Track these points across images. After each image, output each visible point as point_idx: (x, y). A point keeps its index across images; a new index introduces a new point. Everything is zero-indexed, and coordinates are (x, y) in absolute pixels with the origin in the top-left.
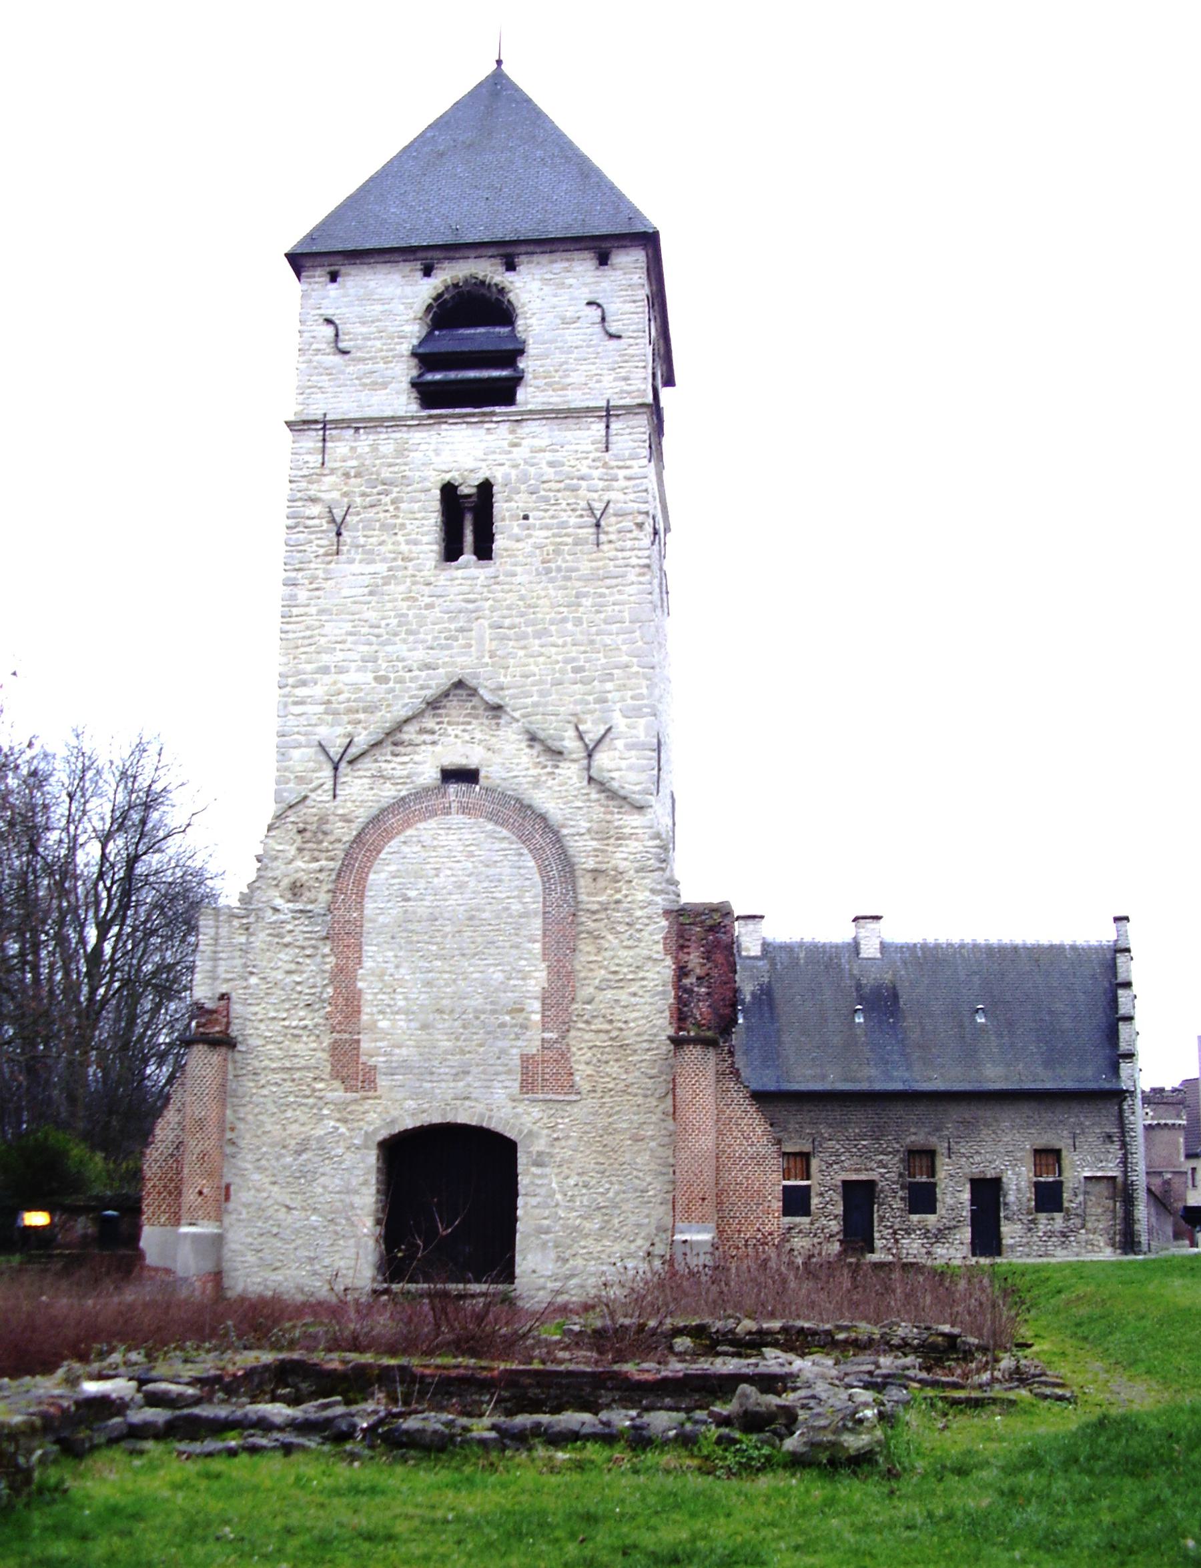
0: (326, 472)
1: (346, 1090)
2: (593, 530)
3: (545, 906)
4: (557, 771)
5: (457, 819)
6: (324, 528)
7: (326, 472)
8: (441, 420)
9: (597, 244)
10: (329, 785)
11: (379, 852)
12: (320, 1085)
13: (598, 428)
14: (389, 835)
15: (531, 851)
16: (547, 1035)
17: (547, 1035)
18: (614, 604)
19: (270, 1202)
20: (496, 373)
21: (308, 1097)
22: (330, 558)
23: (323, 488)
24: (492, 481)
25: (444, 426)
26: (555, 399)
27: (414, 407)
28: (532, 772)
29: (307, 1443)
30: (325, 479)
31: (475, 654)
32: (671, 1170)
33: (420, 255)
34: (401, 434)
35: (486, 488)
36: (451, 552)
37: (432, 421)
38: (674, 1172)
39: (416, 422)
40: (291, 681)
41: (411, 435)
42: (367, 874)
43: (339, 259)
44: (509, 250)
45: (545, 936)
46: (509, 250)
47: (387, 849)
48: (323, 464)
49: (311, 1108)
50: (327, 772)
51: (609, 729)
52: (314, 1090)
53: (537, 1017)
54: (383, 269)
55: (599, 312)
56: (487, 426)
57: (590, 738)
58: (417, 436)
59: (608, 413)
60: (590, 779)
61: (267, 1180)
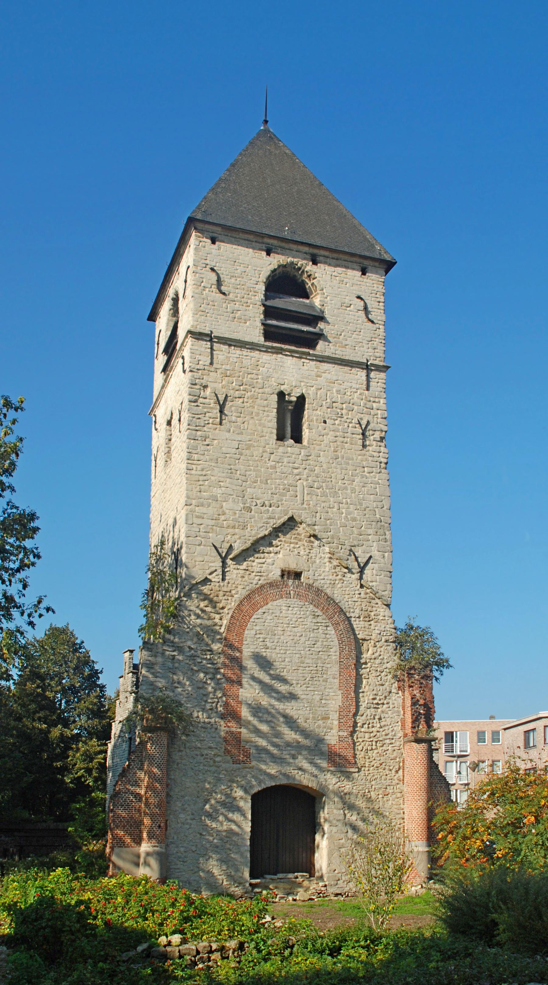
0: (213, 369)
1: (234, 763)
2: (361, 436)
3: (340, 658)
4: (344, 578)
5: (294, 601)
6: (211, 406)
7: (213, 369)
8: (279, 351)
9: (361, 260)
10: (220, 571)
11: (250, 617)
12: (218, 759)
13: (363, 373)
14: (255, 608)
15: (333, 625)
16: (341, 733)
17: (341, 733)
18: (371, 483)
19: (191, 831)
20: (305, 328)
21: (211, 766)
22: (215, 426)
23: (210, 380)
24: (306, 395)
25: (280, 356)
26: (340, 353)
27: (261, 340)
28: (331, 577)
29: (314, 959)
30: (211, 374)
31: (299, 502)
32: (402, 812)
33: (266, 240)
34: (256, 354)
35: (302, 399)
36: (281, 437)
37: (273, 351)
38: (404, 813)
39: (264, 349)
40: (194, 502)
41: (260, 356)
42: (244, 630)
43: (219, 229)
44: (316, 251)
45: (340, 676)
46: (316, 251)
47: (254, 616)
48: (211, 363)
49: (214, 773)
50: (218, 564)
51: (371, 557)
52: (215, 762)
53: (336, 723)
54: (182, 255)
55: (362, 303)
56: (303, 360)
57: (362, 560)
58: (266, 357)
59: (367, 367)
60: (362, 586)
61: (188, 817)
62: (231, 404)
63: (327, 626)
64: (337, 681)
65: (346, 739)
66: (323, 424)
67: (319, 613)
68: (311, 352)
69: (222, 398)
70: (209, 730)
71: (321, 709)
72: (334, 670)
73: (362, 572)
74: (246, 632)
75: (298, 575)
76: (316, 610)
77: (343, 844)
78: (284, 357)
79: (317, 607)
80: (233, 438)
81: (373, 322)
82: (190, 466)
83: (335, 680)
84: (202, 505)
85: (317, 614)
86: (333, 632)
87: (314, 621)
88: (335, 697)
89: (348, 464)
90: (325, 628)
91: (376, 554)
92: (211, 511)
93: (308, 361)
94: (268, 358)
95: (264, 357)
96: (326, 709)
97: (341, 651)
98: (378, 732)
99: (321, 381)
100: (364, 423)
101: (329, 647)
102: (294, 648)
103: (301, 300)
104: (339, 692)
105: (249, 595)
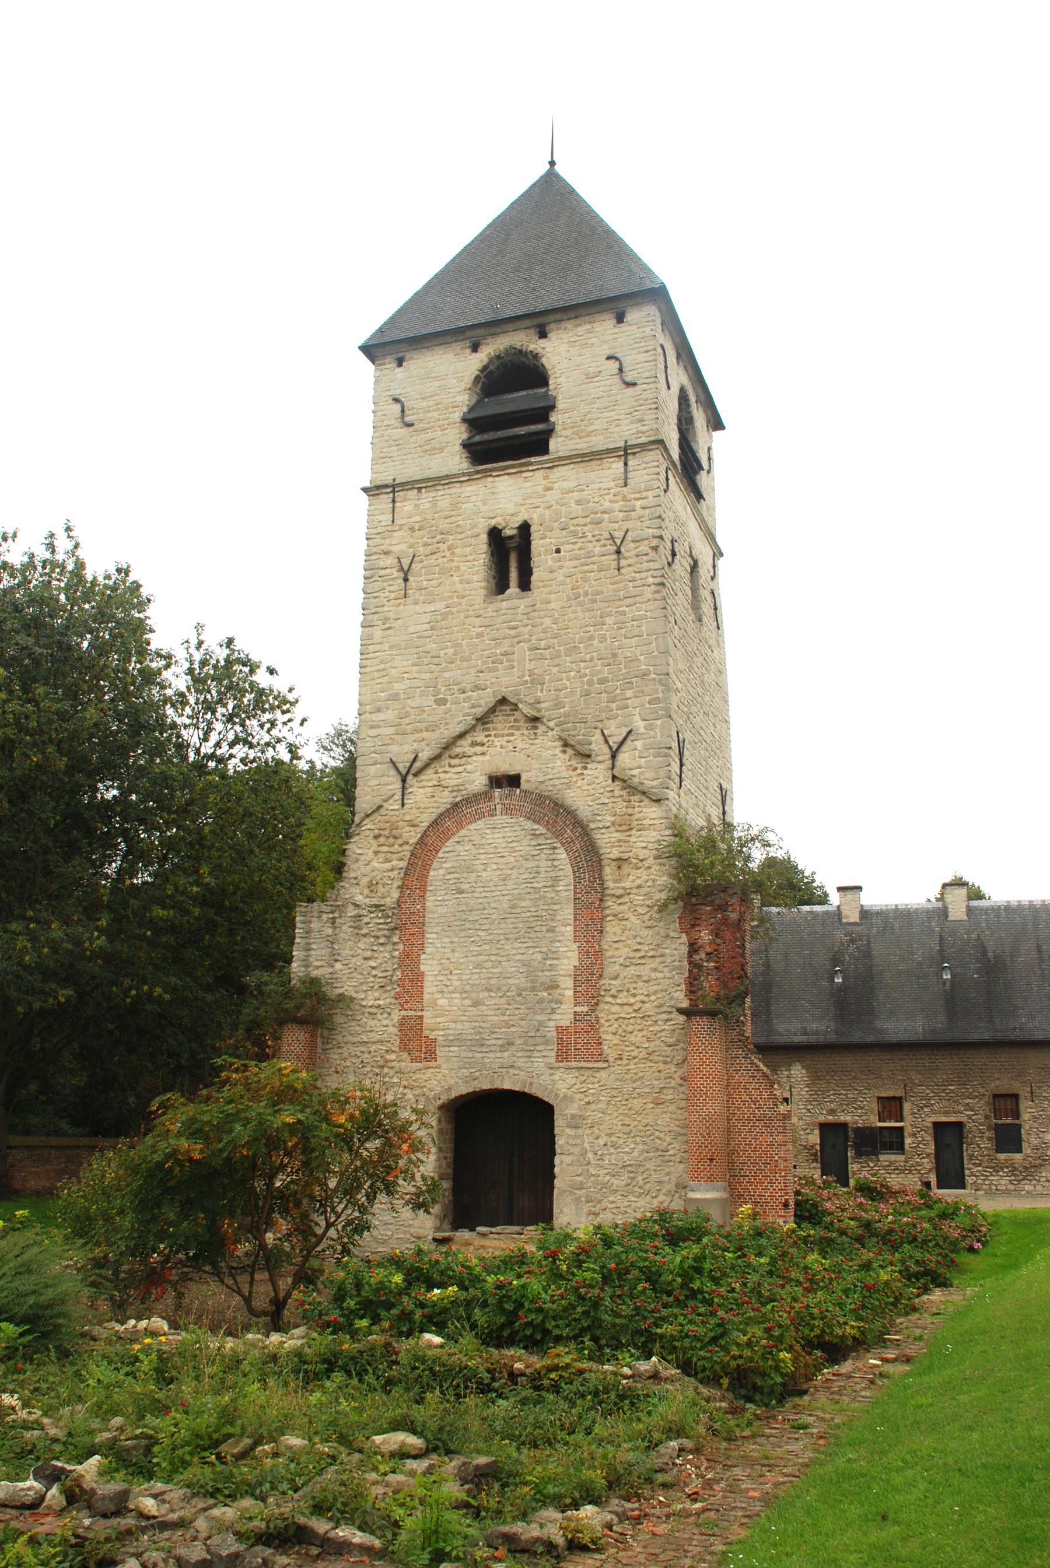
0: (397, 528)
3: (575, 893)
4: (585, 772)
5: (501, 819)
7: (397, 528)
10: (398, 796)
14: (446, 836)
15: (563, 845)
16: (578, 1009)
17: (578, 1009)
24: (529, 521)
25: (490, 479)
26: (582, 445)
30: (395, 534)
33: (468, 334)
35: (525, 528)
42: (428, 871)
45: (575, 920)
50: (398, 785)
51: (630, 732)
53: (570, 993)
57: (613, 741)
60: (614, 778)
62: (420, 565)
63: (555, 848)
64: (570, 929)
65: (586, 1018)
66: (555, 555)
67: (542, 830)
68: (546, 457)
69: (406, 563)
70: (379, 1016)
71: (547, 973)
72: (567, 912)
73: (614, 757)
74: (432, 873)
75: (513, 780)
76: (536, 827)
77: (581, 1182)
78: (497, 479)
79: (539, 823)
80: (423, 610)
81: (634, 384)
82: (365, 663)
83: (569, 928)
84: (379, 710)
85: (537, 832)
86: (564, 856)
87: (534, 843)
88: (569, 954)
89: (595, 601)
90: (551, 852)
91: (640, 725)
92: (389, 715)
93: (531, 474)
94: (473, 488)
95: (469, 489)
96: (553, 973)
97: (577, 880)
98: (643, 1002)
99: (553, 496)
100: (619, 535)
101: (556, 879)
102: (503, 888)
103: (535, 391)
104: (575, 946)
105: (435, 821)
